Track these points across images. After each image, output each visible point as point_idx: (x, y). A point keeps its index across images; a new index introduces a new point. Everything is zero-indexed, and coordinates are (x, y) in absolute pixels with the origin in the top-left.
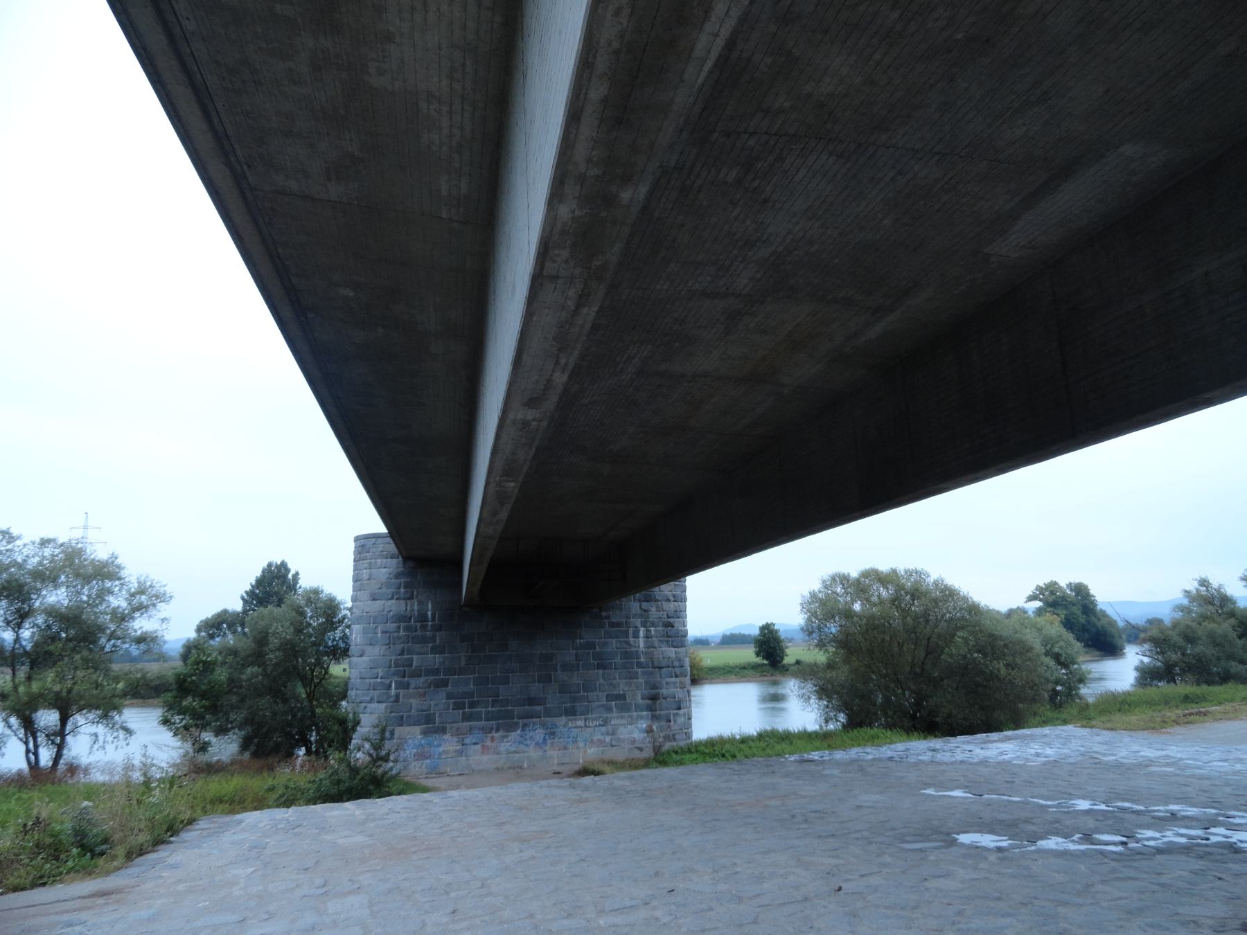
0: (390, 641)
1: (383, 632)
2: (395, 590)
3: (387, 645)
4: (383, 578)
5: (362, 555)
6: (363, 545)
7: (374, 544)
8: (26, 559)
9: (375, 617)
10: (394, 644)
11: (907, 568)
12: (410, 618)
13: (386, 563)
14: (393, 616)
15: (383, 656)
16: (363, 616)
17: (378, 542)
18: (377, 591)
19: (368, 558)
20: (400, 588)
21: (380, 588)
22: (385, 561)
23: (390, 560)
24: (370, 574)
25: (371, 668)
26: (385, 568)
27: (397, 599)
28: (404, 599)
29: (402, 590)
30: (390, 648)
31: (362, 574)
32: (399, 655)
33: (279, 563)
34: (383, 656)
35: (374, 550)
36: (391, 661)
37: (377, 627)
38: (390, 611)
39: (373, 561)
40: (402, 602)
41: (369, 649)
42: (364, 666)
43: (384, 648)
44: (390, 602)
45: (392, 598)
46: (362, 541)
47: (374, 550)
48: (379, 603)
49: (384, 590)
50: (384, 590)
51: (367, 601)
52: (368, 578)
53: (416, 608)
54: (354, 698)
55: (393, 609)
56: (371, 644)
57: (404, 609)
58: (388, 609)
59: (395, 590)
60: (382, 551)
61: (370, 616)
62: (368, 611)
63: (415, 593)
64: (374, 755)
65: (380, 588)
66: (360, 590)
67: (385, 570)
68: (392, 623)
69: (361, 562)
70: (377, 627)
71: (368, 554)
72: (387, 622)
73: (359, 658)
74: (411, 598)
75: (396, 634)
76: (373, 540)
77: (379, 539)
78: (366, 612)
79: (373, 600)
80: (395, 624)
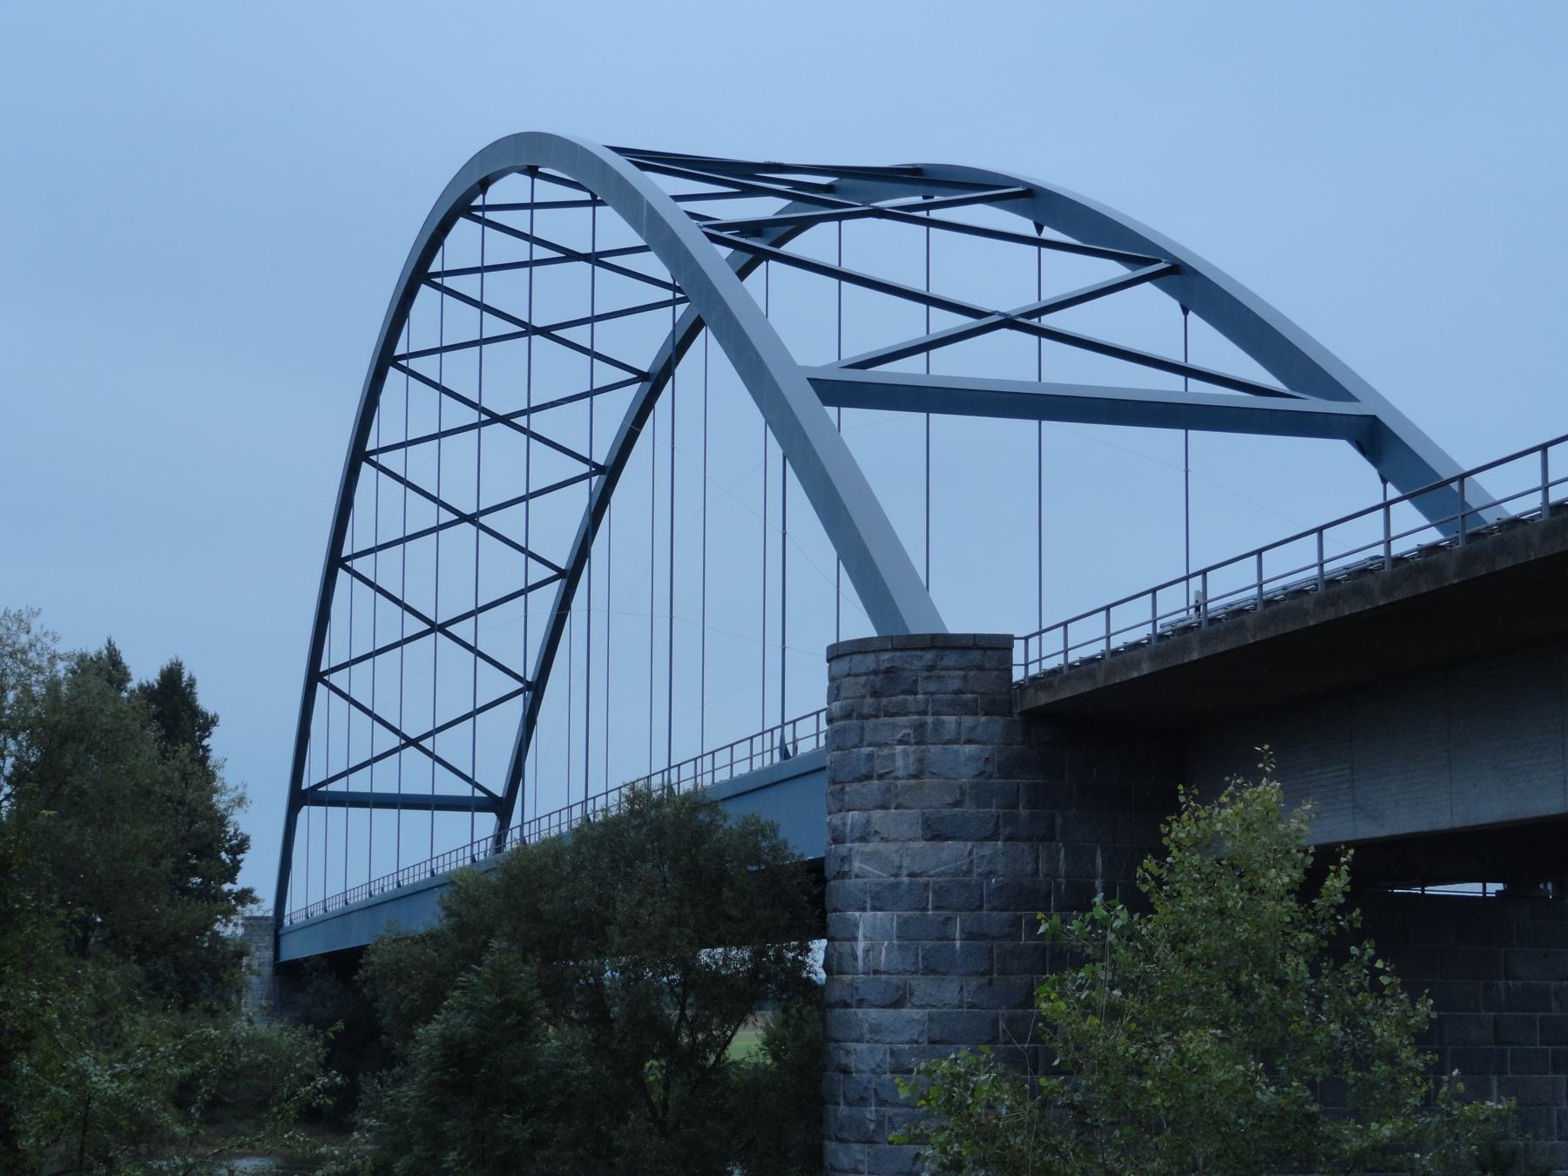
0: (992, 964)
1: (969, 936)
2: (1002, 812)
3: (983, 974)
4: (966, 775)
5: (884, 701)
6: (888, 671)
7: (931, 668)
8: (1256, 1117)
9: (941, 892)
10: (1002, 973)
11: (184, 665)
12: (1048, 895)
13: (973, 728)
14: (999, 889)
15: (973, 1006)
16: (896, 886)
17: (945, 663)
18: (946, 811)
19: (912, 708)
20: (1016, 806)
21: (957, 804)
22: (968, 720)
23: (983, 719)
24: (921, 761)
25: (932, 1042)
26: (969, 742)
27: (1009, 838)
28: (1029, 839)
29: (1023, 812)
30: (990, 983)
31: (892, 757)
32: (1020, 1006)
33: (159, 678)
34: (973, 1006)
35: (932, 687)
36: (995, 1022)
37: (948, 919)
38: (990, 874)
39: (930, 719)
40: (1023, 846)
41: (922, 986)
42: (913, 1033)
43: (974, 982)
44: (988, 849)
45: (994, 836)
46: (886, 656)
47: (932, 687)
48: (950, 849)
49: (969, 809)
50: (969, 809)
51: (914, 839)
52: (912, 770)
53: (1062, 866)
54: (872, 1126)
55: (1000, 868)
56: (929, 971)
57: (1029, 868)
58: (984, 868)
59: (1002, 812)
60: (957, 692)
61: (926, 885)
62: (916, 869)
63: (1059, 821)
64: (465, 1012)
65: (957, 804)
66: (884, 807)
67: (969, 749)
68: (993, 909)
69: (883, 720)
70: (948, 919)
71: (910, 698)
72: (980, 907)
73: (890, 1012)
74: (1048, 837)
75: (1008, 944)
76: (929, 656)
77: (854, 656)
78: (910, 875)
79: (932, 839)
80: (1005, 914)
